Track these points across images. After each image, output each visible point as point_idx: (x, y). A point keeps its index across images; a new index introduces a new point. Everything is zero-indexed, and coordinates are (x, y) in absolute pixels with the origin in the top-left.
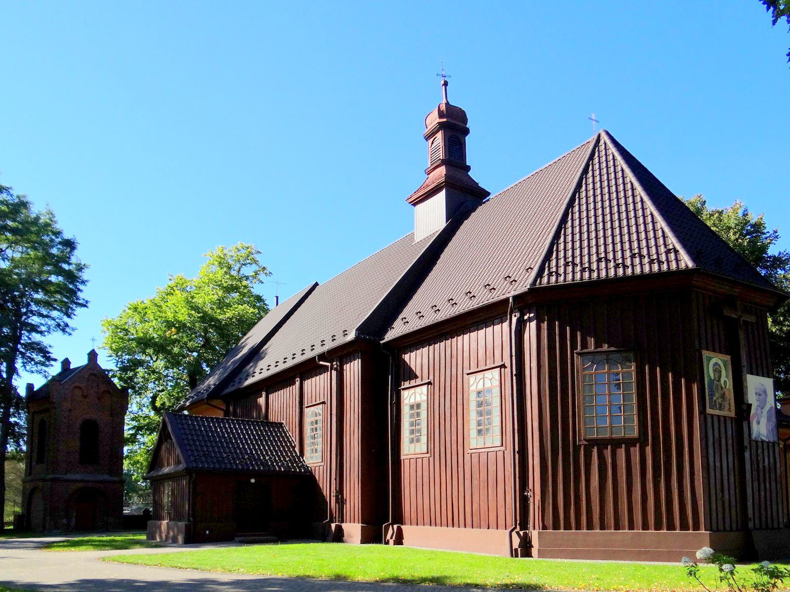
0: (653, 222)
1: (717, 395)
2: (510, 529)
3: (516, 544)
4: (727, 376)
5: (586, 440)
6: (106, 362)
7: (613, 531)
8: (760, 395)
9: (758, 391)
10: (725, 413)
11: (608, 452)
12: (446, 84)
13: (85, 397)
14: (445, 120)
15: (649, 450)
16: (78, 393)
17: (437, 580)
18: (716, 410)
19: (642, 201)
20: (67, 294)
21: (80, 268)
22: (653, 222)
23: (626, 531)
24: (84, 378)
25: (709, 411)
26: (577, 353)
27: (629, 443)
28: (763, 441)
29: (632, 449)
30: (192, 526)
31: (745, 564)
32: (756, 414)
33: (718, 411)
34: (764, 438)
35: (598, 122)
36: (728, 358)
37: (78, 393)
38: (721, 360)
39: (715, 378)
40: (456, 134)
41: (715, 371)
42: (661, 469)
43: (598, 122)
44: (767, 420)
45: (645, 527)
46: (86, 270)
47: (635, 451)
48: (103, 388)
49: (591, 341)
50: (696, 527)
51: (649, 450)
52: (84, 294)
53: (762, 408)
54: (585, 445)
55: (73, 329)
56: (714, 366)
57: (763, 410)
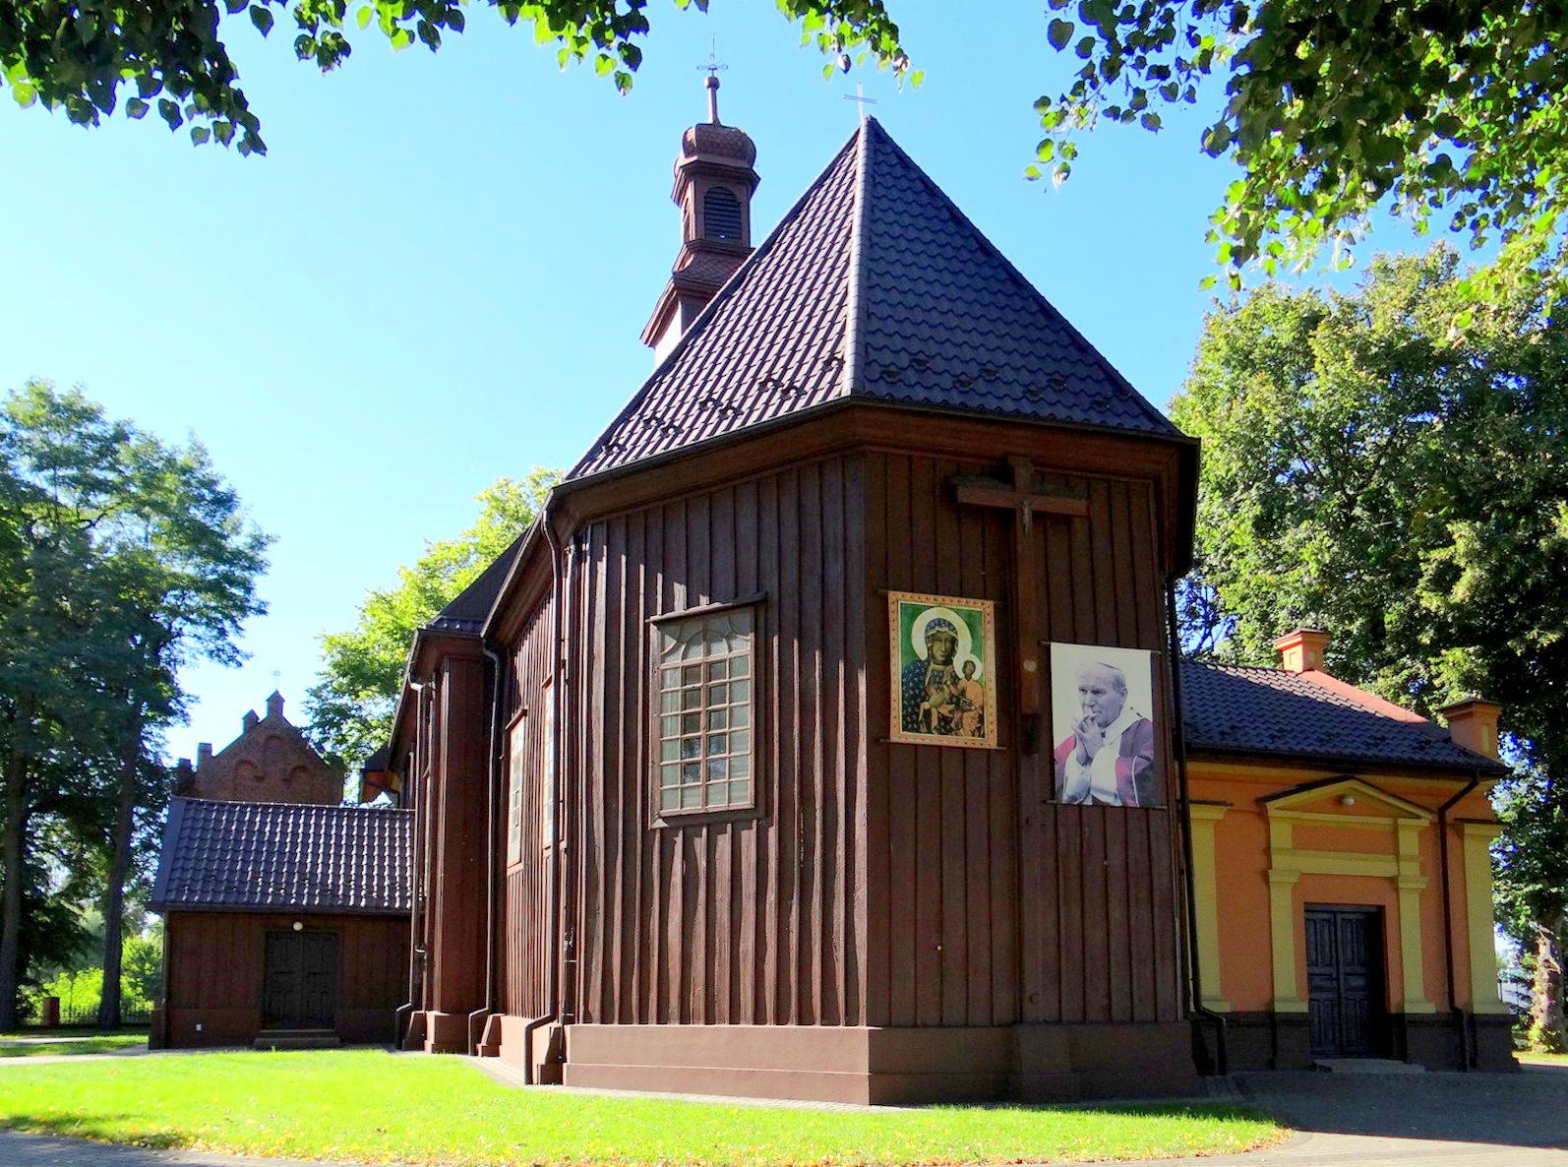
0: (841, 306)
1: (935, 697)
2: (531, 1021)
3: (540, 1057)
4: (977, 650)
5: (665, 819)
6: (297, 715)
7: (794, 1026)
8: (1096, 692)
9: (1092, 683)
10: (962, 740)
11: (700, 844)
12: (714, 84)
13: (260, 779)
14: (695, 158)
15: (773, 833)
16: (246, 772)
17: (54, 1126)
18: (929, 731)
19: (847, 262)
20: (229, 595)
21: (259, 543)
22: (841, 306)
23: (635, 1025)
24: (257, 743)
25: (898, 734)
26: (655, 623)
27: (735, 820)
28: (1103, 807)
29: (744, 833)
30: (163, 1017)
31: (1063, 1110)
32: (1079, 739)
33: (936, 735)
34: (1104, 799)
35: (848, 97)
36: (986, 608)
37: (246, 772)
38: (957, 612)
39: (931, 656)
40: (723, 185)
41: (931, 639)
42: (794, 880)
43: (848, 97)
44: (1122, 752)
45: (759, 1019)
46: (270, 547)
47: (749, 837)
48: (294, 761)
49: (680, 590)
50: (851, 1021)
51: (773, 833)
52: (263, 587)
53: (1105, 724)
54: (662, 830)
55: (247, 657)
56: (930, 627)
57: (1109, 731)
